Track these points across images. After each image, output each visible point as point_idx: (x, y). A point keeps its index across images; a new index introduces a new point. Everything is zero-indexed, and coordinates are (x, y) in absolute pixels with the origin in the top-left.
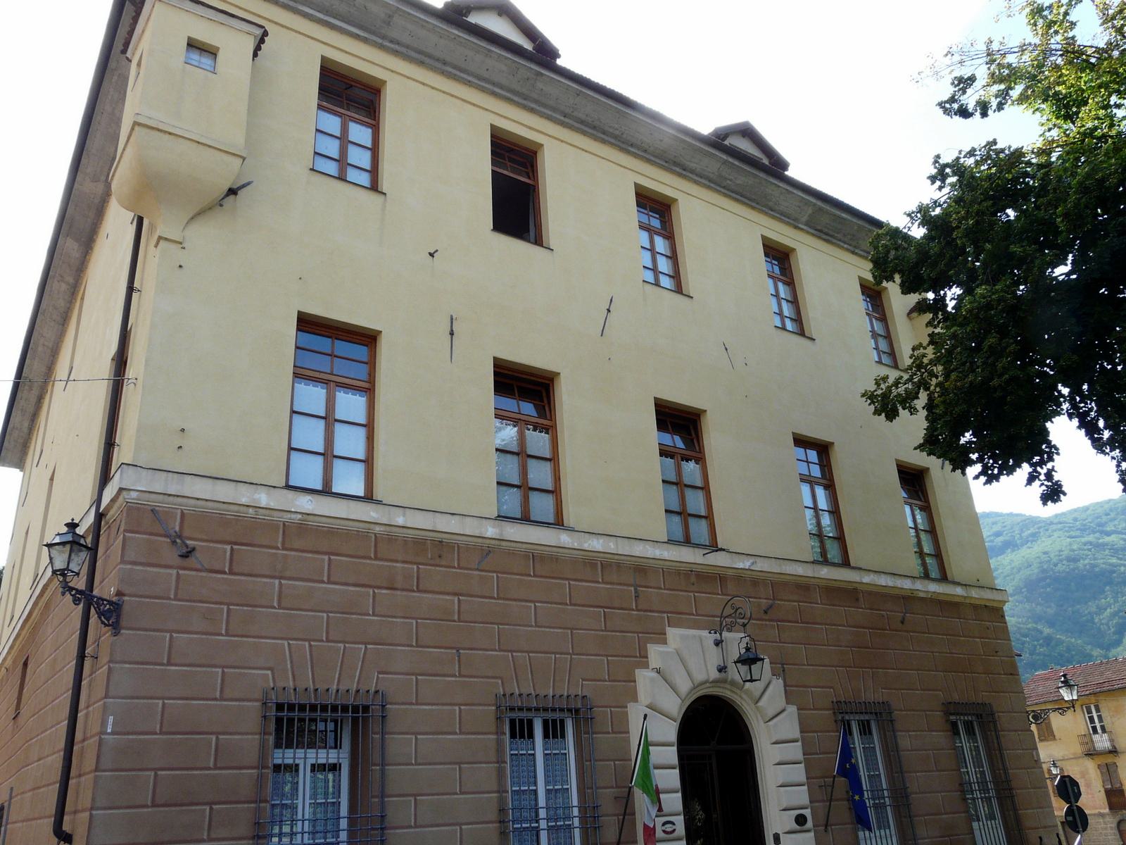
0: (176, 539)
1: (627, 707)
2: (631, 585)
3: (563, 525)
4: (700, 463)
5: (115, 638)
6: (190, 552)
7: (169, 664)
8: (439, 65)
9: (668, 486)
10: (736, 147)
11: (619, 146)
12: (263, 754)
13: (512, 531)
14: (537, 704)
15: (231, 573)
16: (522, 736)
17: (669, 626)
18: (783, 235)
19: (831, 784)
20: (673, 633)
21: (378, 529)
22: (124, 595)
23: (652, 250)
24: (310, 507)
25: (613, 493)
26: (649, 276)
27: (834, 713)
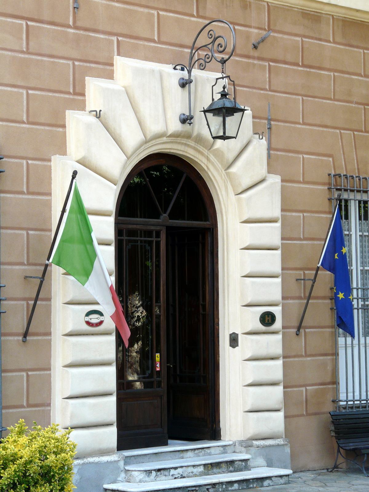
1: (50, 160)
17: (119, 54)
19: (313, 278)
20: (123, 65)
27: (329, 189)
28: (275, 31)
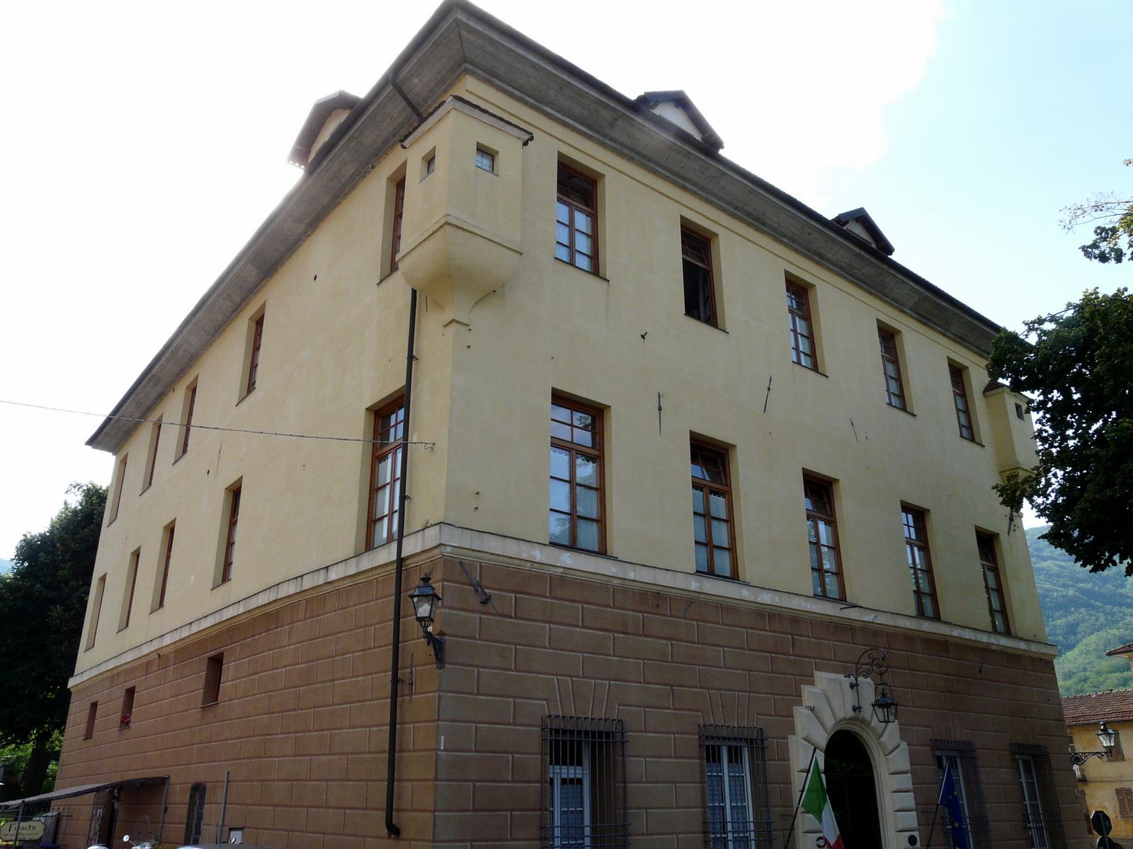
0: (478, 587)
1: (787, 739)
2: (789, 634)
3: (738, 580)
4: (727, 496)
5: (441, 671)
6: (488, 599)
7: (478, 694)
8: (643, 161)
9: (698, 517)
10: (851, 231)
11: (775, 237)
12: (544, 771)
13: (709, 585)
14: (564, 726)
15: (516, 618)
16: (714, 761)
17: (816, 670)
18: (894, 319)
19: (935, 811)
20: (820, 676)
21: (615, 582)
22: (445, 634)
23: (571, 226)
24: (571, 563)
25: (775, 554)
26: (563, 254)
27: (932, 749)
28: (892, 649)
